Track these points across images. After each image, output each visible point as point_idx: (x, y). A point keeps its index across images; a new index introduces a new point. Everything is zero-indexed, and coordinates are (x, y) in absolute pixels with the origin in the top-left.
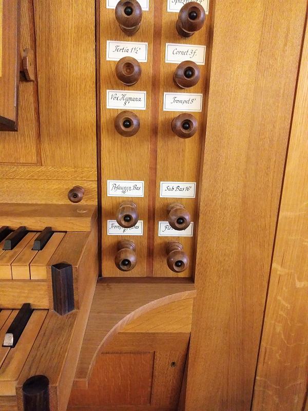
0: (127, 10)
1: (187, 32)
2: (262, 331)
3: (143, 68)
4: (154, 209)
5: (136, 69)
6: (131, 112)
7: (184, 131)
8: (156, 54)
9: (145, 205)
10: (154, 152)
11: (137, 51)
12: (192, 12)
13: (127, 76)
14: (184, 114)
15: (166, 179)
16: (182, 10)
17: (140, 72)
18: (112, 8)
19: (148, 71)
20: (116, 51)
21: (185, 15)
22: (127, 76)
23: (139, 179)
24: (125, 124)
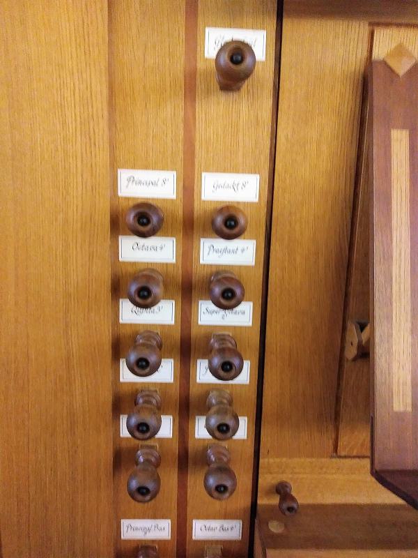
4: (192, 212)
10: (182, 486)
13: (145, 220)
15: (198, 518)
21: (225, 59)
22: (145, 220)
23: (164, 517)
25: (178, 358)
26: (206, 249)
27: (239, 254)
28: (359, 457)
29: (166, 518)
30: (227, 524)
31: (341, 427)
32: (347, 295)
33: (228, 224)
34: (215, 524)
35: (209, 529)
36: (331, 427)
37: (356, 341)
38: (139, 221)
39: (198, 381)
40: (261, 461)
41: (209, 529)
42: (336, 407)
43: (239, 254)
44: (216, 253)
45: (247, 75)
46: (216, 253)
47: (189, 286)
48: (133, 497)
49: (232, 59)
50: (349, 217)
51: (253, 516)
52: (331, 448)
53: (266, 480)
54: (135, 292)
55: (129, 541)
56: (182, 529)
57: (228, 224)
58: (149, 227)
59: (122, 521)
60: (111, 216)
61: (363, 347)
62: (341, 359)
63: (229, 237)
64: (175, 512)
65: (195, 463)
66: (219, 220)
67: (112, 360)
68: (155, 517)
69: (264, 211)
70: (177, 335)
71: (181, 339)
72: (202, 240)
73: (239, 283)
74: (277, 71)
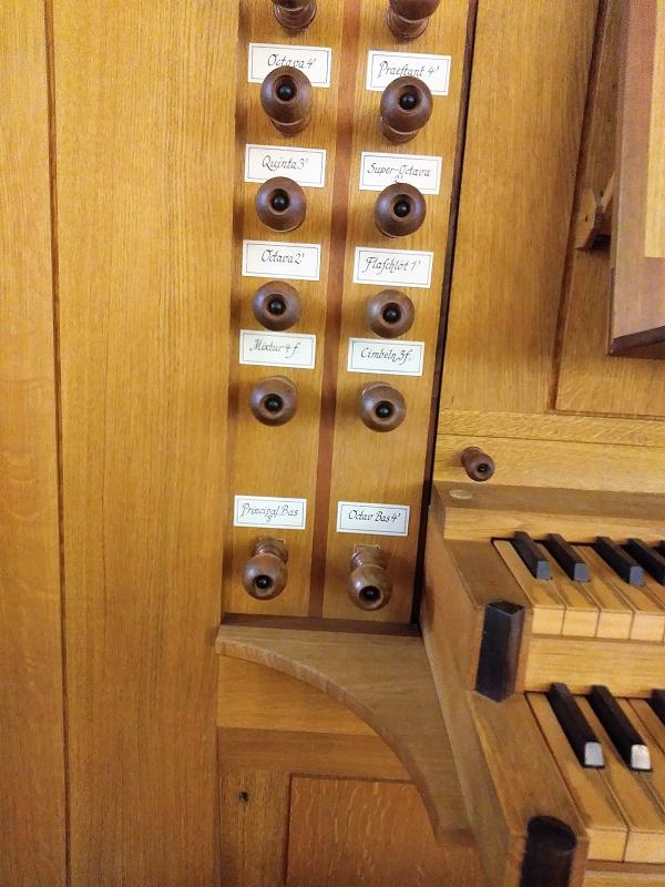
0: (282, 90)
1: (409, 22)
2: (537, 720)
3: (310, 198)
4: (334, 392)
5: (294, 202)
6: (287, 285)
7: (376, 419)
8: (341, 174)
9: (322, 297)
10: (326, 447)
11: (306, 167)
12: (402, 97)
13: (276, 309)
14: (392, 292)
15: (346, 499)
16: (383, 194)
17: (303, 207)
18: (257, 81)
19: (324, 206)
20: (265, 163)
21: (392, 100)
22: (276, 309)
23: (295, 495)
24: (272, 403)
25: (327, 242)
26: (377, 68)
27: (407, 268)
28: (588, 414)
29: (301, 497)
30: (388, 510)
31: (563, 365)
32: (582, 154)
33: (391, 317)
34: (371, 509)
35: (362, 517)
36: (548, 364)
37: (594, 205)
38: (269, 306)
39: (355, 281)
40: (441, 413)
41: (362, 517)
42: (557, 335)
43: (407, 268)
44: (367, 358)
45: (422, 121)
46: (367, 358)
47: (337, 322)
48: (252, 594)
49: (402, 103)
50: (592, 24)
51: (427, 500)
52: (547, 399)
53: (448, 445)
54: (263, 303)
55: (243, 529)
56: (322, 514)
57: (391, 317)
58: (279, 414)
59: (236, 497)
60: (232, 302)
61: (603, 215)
62: (571, 240)
63: (386, 334)
64: (311, 482)
65: (345, 412)
66: (376, 309)
67: (231, 328)
68: (283, 494)
69: (437, 298)
70: (318, 386)
71: (333, 217)
72: (371, 53)
73: (400, 399)
74: (435, 406)
